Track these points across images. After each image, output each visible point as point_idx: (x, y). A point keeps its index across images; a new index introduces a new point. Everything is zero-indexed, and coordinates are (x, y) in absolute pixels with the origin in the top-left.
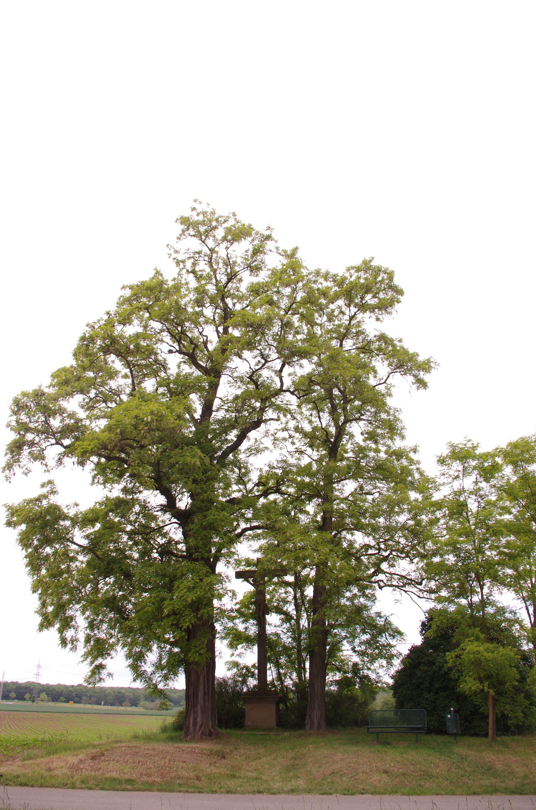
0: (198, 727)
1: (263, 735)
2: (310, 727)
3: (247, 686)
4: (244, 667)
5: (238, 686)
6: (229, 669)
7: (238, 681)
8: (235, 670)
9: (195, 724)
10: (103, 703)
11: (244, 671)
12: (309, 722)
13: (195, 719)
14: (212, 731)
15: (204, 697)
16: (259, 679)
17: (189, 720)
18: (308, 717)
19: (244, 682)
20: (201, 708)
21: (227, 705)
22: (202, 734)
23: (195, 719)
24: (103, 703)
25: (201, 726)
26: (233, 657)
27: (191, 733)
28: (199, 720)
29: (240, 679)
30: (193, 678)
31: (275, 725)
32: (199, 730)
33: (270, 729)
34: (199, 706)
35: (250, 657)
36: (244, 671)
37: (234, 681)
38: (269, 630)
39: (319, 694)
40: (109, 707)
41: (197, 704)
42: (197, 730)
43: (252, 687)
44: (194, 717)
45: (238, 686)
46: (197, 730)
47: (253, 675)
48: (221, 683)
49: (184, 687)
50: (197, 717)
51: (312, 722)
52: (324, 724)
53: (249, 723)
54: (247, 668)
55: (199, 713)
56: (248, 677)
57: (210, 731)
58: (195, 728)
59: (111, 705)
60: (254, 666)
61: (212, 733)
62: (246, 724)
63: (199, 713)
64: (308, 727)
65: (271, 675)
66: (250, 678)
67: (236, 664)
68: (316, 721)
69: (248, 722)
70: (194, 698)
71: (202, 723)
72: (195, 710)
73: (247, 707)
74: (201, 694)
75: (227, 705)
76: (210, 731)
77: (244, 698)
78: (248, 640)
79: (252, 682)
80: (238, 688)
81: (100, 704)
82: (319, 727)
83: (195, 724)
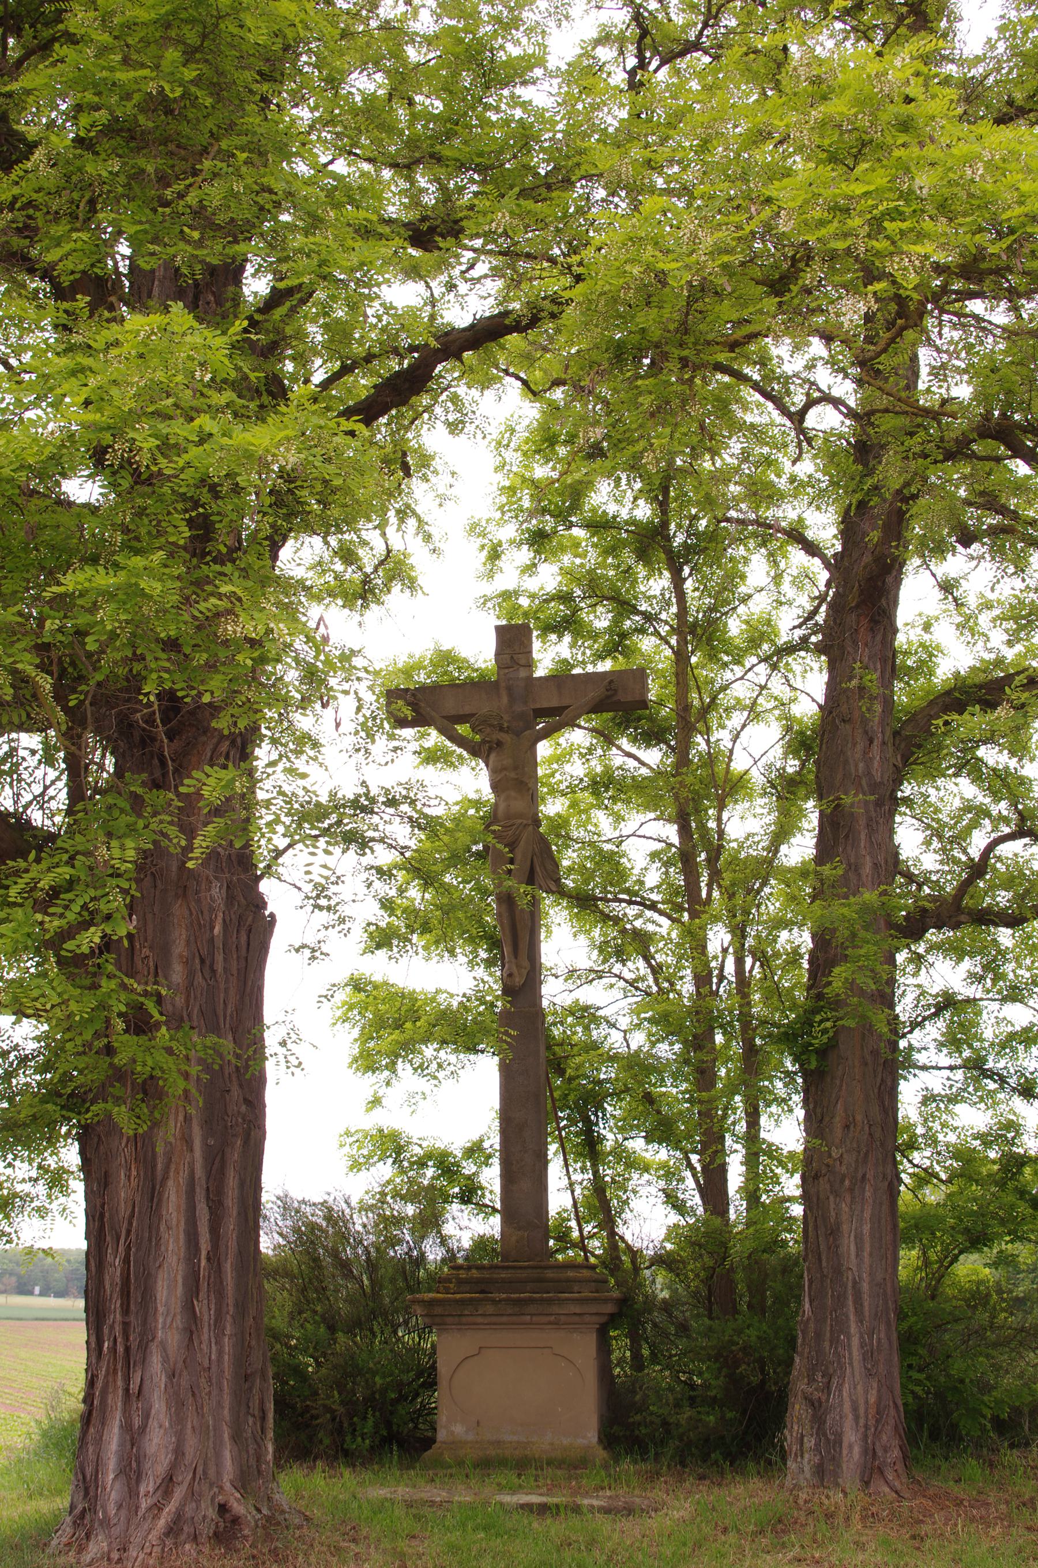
0: (148, 1485)
1: (543, 1509)
2: (820, 1471)
3: (444, 1241)
4: (429, 1156)
5: (400, 1241)
6: (356, 1166)
7: (398, 1221)
8: (385, 1170)
9: (132, 1470)
10: (37, 1290)
11: (430, 1172)
12: (810, 1442)
13: (134, 1436)
14: (238, 1508)
15: (189, 1309)
16: (509, 1212)
17: (99, 1441)
18: (798, 1410)
19: (430, 1222)
20: (172, 1375)
21: (341, 1337)
22: (173, 1530)
23: (134, 1436)
24: (37, 1290)
25: (168, 1483)
26: (378, 1110)
27: (106, 1523)
28: (157, 1442)
29: (410, 1210)
30: (125, 1190)
31: (591, 1436)
32: (157, 1508)
33: (573, 1465)
34: (156, 1362)
35: (461, 1103)
36: (430, 1172)
37: (384, 1219)
38: (554, 993)
39: (865, 1286)
40: (52, 1301)
41: (144, 1347)
42: (144, 1504)
43: (466, 1244)
44: (127, 1427)
45: (400, 1241)
46: (144, 1504)
47: (470, 1194)
48: (313, 1227)
49: (83, 1245)
50: (143, 1428)
51: (830, 1446)
52: (896, 1453)
53: (458, 1429)
54: (447, 1166)
55: (159, 1405)
56: (447, 1199)
57: (223, 1509)
58: (132, 1493)
59: (59, 1294)
60: (474, 1151)
61: (236, 1520)
62: (442, 1435)
63: (159, 1405)
64: (800, 1467)
65: (562, 1190)
66: (455, 1207)
67: (391, 1145)
68: (851, 1436)
69: (452, 1427)
70: (126, 1311)
71: (174, 1466)
72: (134, 1387)
73: (450, 1349)
74: (168, 1290)
75: (341, 1337)
76: (223, 1509)
77: (432, 1303)
78: (459, 1031)
79: (467, 1227)
80: (400, 1250)
81: (31, 1293)
82: (871, 1471)
83: (132, 1470)
